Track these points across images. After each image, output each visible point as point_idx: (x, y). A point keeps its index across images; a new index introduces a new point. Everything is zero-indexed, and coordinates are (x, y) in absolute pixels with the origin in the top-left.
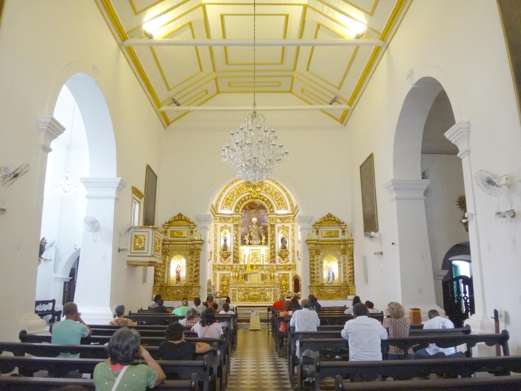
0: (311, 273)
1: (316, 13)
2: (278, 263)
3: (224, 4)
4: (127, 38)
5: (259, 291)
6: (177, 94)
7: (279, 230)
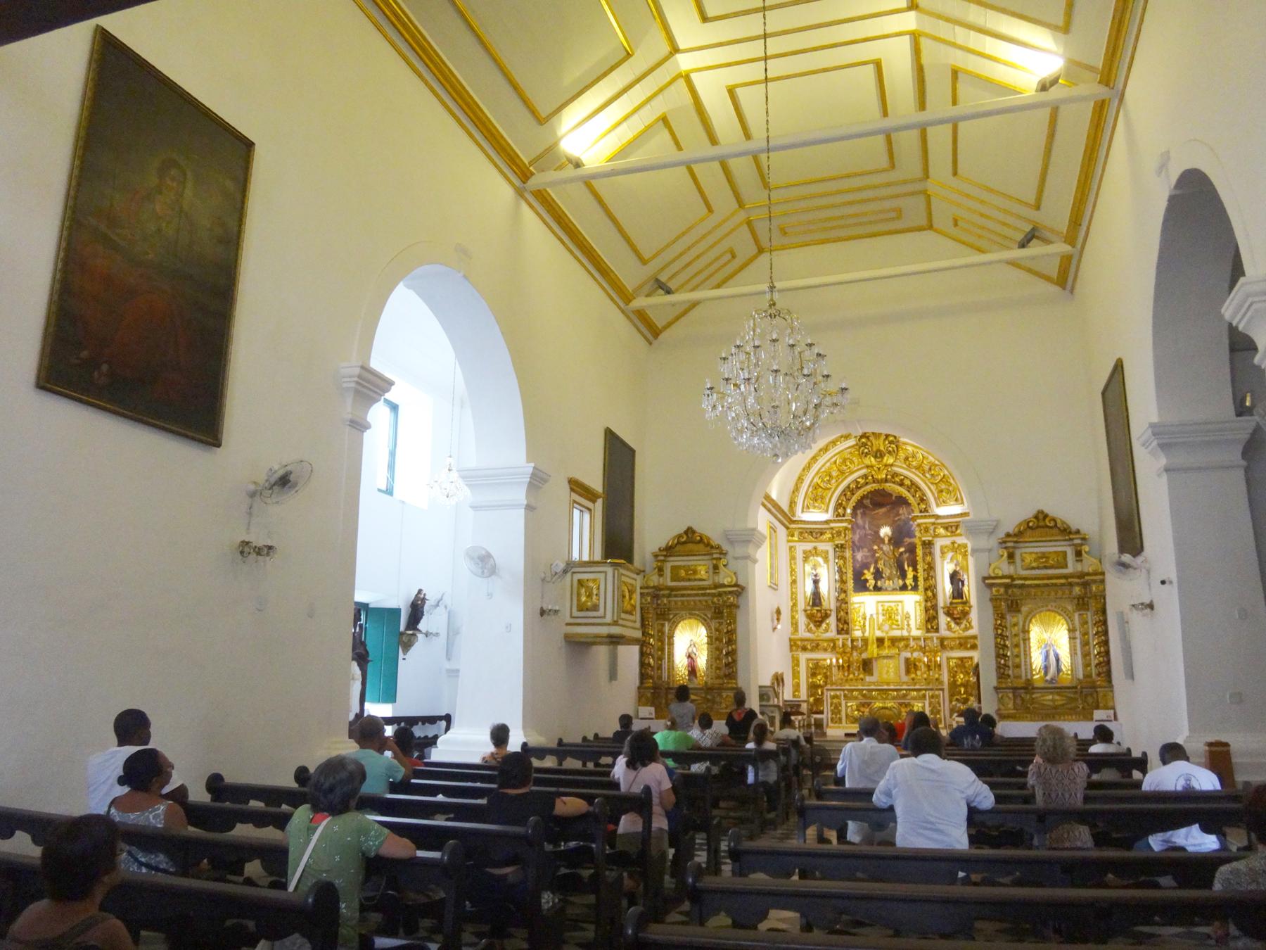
0: (998, 656)
1: (943, 46)
2: (943, 632)
3: (729, 65)
4: (532, 174)
5: (894, 698)
6: (663, 269)
7: (943, 553)
